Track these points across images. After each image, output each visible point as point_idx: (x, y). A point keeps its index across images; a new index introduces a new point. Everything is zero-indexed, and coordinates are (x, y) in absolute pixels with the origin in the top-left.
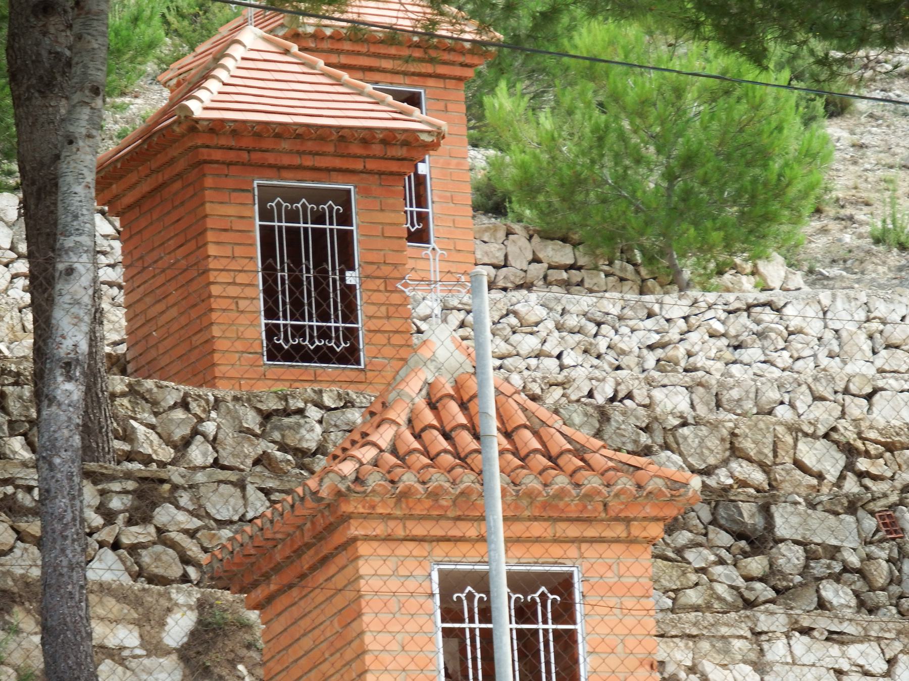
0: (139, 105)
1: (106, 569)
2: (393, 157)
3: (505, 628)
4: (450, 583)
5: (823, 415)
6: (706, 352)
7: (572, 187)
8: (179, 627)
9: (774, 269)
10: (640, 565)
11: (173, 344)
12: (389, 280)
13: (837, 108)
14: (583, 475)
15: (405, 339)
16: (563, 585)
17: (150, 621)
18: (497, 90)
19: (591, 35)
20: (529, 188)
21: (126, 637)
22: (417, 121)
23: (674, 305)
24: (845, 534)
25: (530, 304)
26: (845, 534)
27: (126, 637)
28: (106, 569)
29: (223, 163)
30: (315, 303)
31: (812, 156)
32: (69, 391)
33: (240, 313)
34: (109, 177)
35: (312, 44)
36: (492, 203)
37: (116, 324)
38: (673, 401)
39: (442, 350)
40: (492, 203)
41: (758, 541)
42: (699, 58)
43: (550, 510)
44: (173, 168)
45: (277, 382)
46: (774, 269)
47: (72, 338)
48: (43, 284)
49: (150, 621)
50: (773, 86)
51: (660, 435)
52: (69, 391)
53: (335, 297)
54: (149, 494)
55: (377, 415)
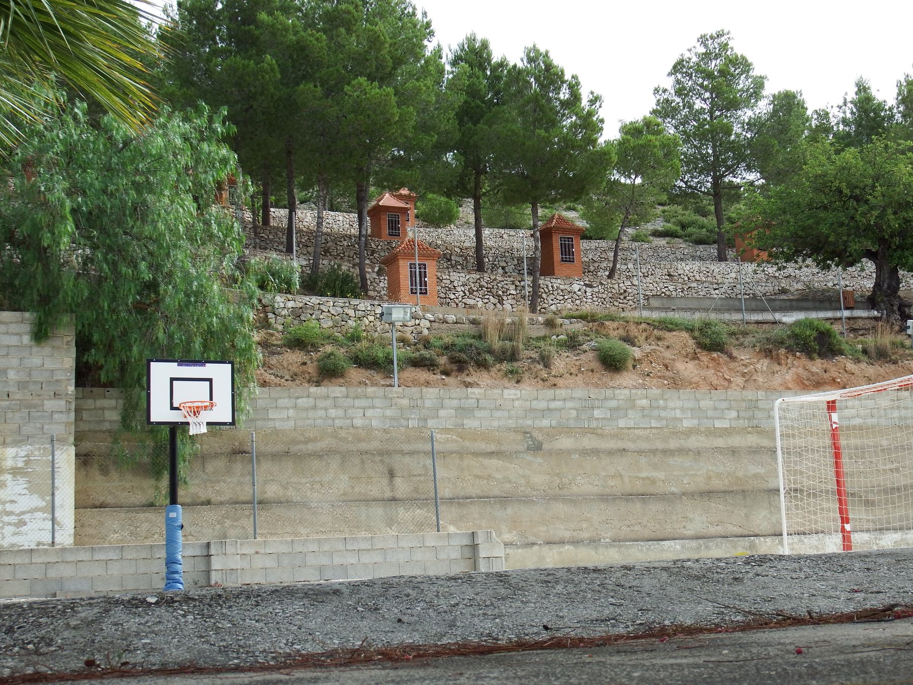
0: (374, 203)
1: (367, 262)
2: (404, 211)
3: (418, 270)
4: (411, 264)
5: (458, 244)
6: (444, 236)
7: (427, 215)
8: (376, 269)
9: (452, 226)
10: (435, 263)
11: (376, 233)
12: (403, 226)
13: (461, 206)
14: (428, 252)
15: (406, 234)
16: (425, 265)
17: (373, 268)
18: (35, 496)
19: (430, 196)
20: (422, 215)
21: (370, 270)
22: (408, 206)
23: (440, 230)
24: (460, 260)
25: (422, 229)
26: (460, 260)
27: (370, 270)
28: (367, 262)
29: (664, 498)
30: (395, 229)
31: (458, 212)
32: (363, 239)
33: (385, 230)
34: (369, 213)
35: (395, 196)
36: (417, 217)
37: (369, 231)
38: (439, 242)
39: (410, 234)
40: (417, 217)
41: (450, 260)
42: (443, 199)
43: (423, 256)
44: (377, 212)
45: (389, 238)
46: (452, 226)
47: (364, 232)
48: (360, 225)
49: (373, 268)
50: (453, 203)
51: (438, 246)
52: (363, 239)
53: (423, 283)
54: (373, 252)
55: (402, 243)
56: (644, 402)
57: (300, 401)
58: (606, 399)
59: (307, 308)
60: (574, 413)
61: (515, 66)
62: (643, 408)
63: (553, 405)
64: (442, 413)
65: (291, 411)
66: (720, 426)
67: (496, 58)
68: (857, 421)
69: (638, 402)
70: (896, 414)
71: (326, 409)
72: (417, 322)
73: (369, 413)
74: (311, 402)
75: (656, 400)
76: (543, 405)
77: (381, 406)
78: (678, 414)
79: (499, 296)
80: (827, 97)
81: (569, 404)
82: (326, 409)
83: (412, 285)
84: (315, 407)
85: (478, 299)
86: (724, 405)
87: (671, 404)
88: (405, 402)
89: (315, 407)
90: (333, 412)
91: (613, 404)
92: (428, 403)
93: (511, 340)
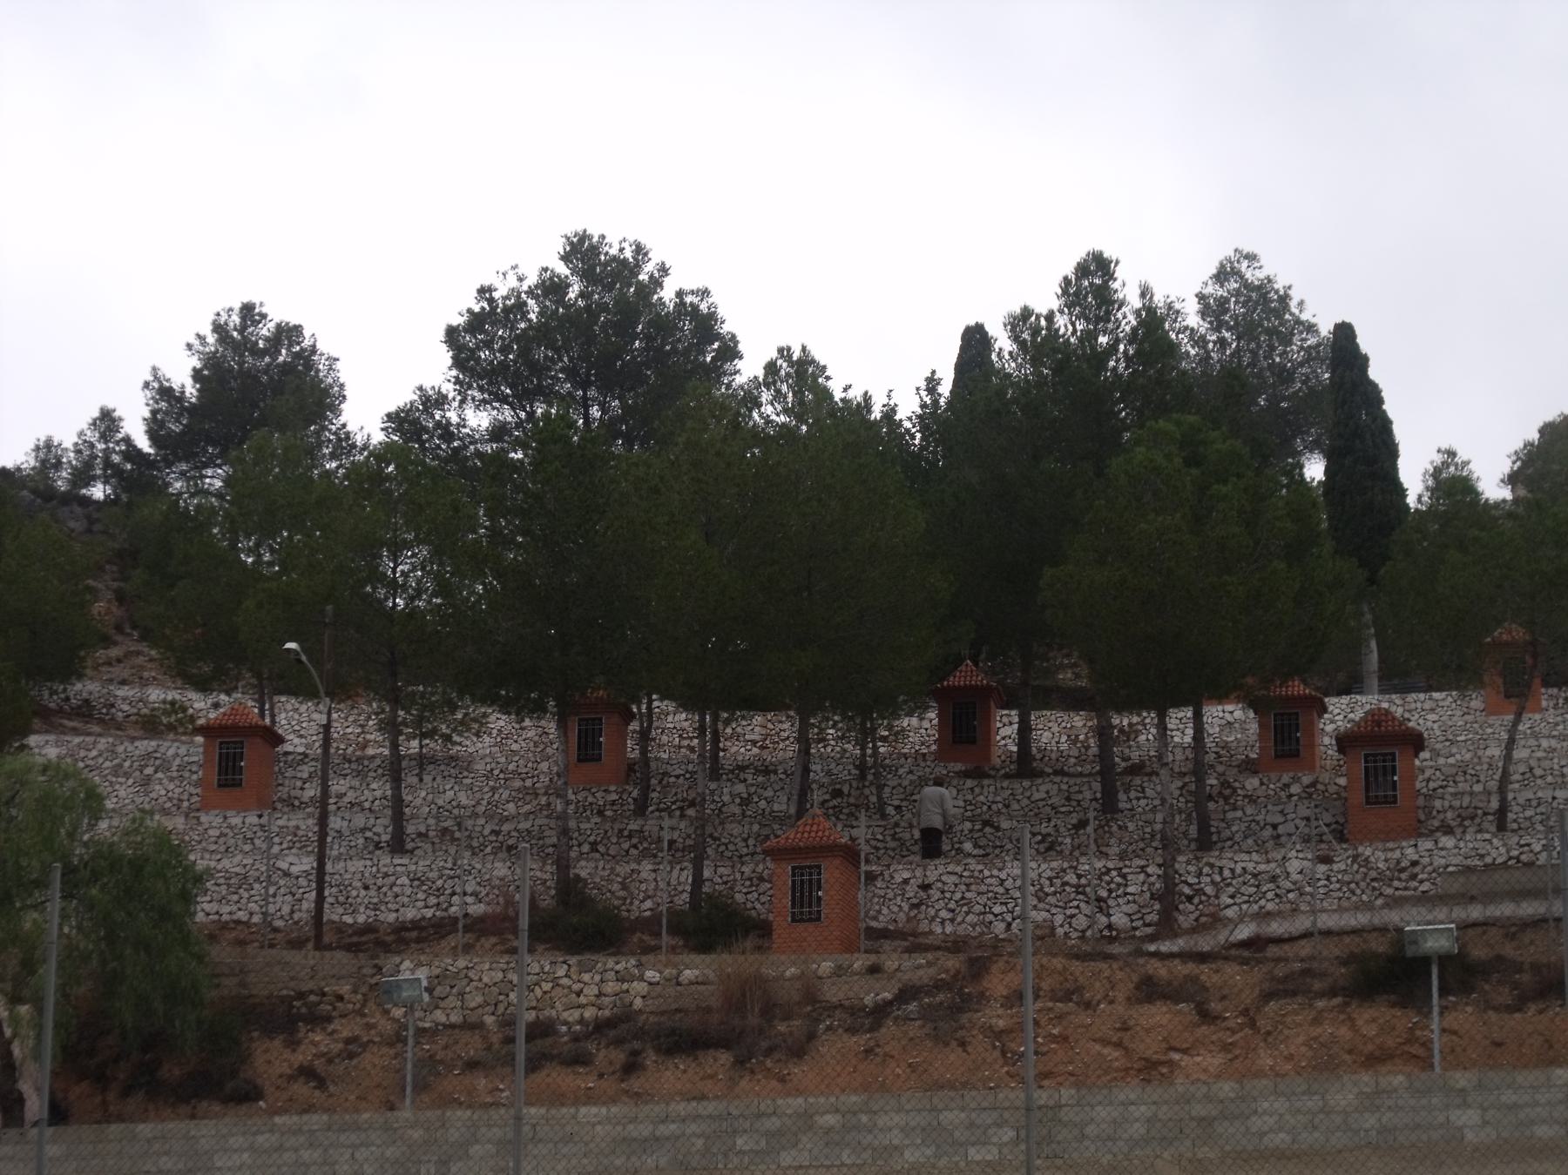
53: (814, 901)
56: (830, 1120)
57: (260, 1139)
58: (760, 1115)
59: (446, 977)
60: (700, 1143)
61: (737, 372)
62: (829, 1130)
63: (663, 1130)
64: (476, 1150)
65: (246, 1155)
66: (978, 1158)
67: (359, 440)
68: (1281, 1139)
69: (817, 1118)
70: (1370, 1121)
71: (296, 1150)
72: (625, 986)
73: (361, 1154)
74: (274, 1139)
75: (855, 1114)
76: (645, 1130)
77: (378, 1142)
78: (896, 1138)
79: (1099, 899)
80: (892, 365)
81: (693, 1128)
82: (296, 1150)
83: (793, 906)
84: (280, 1148)
85: (1054, 911)
86: (988, 1118)
87: (882, 1121)
88: (417, 1134)
89: (280, 1148)
90: (306, 1155)
91: (773, 1123)
92: (454, 1135)
93: (367, 1024)
